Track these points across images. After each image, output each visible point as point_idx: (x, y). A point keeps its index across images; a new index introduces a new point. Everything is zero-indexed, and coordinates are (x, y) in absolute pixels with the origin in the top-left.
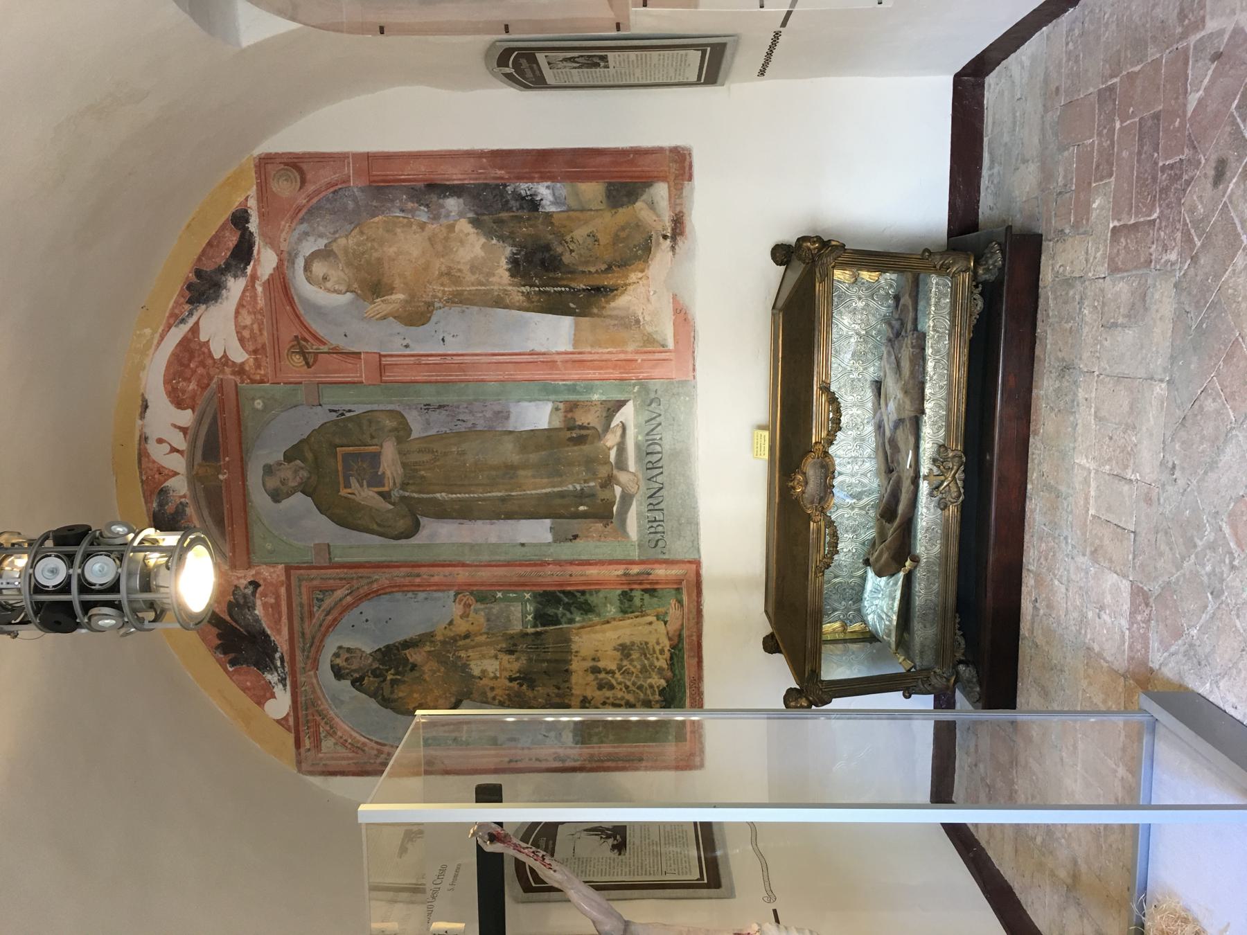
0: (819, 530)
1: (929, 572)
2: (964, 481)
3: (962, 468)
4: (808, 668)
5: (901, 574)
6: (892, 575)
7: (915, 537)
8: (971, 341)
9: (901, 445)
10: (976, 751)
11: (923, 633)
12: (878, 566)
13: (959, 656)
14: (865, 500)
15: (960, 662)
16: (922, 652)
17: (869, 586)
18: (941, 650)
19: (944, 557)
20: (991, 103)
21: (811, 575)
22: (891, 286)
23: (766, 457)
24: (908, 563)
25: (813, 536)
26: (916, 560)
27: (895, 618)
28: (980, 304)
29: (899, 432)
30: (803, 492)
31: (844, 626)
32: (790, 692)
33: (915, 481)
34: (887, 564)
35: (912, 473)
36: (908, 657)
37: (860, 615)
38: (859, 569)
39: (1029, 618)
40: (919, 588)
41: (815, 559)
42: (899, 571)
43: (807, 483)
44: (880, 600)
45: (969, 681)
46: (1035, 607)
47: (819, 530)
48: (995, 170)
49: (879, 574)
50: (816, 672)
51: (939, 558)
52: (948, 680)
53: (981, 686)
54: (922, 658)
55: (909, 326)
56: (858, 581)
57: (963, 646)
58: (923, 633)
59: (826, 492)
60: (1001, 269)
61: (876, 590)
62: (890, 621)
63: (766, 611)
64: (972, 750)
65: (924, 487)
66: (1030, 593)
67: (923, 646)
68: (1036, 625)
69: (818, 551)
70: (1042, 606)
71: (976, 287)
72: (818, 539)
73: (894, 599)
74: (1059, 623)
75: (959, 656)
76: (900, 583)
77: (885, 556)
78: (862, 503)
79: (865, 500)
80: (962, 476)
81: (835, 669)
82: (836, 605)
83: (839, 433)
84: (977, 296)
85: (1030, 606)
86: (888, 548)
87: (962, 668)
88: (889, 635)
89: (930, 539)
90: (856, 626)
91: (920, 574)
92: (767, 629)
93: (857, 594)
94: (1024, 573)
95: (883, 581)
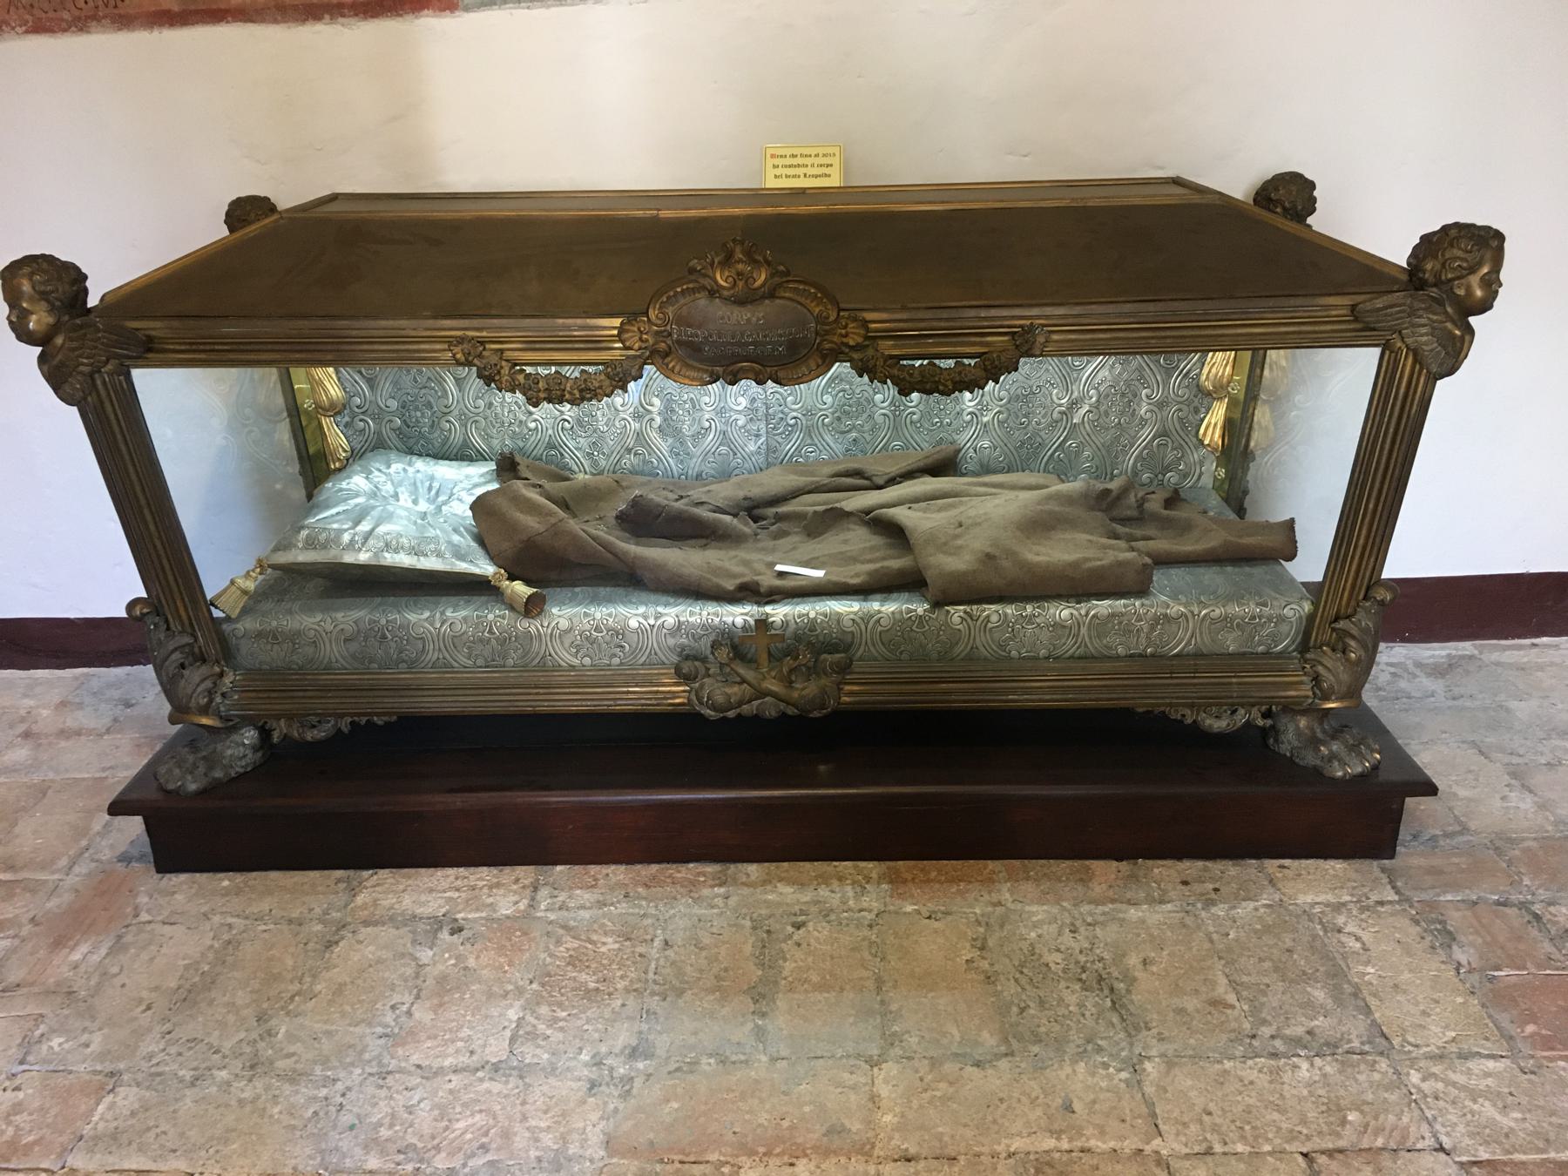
0: (595, 344)
1: (503, 642)
2: (756, 719)
3: (791, 711)
4: (155, 327)
5: (486, 568)
6: (480, 541)
7: (595, 600)
8: (1128, 712)
9: (832, 543)
10: (64, 734)
11: (330, 627)
12: (503, 504)
13: (280, 729)
14: (662, 445)
15: (265, 733)
16: (273, 636)
17: (446, 471)
18: (281, 683)
19: (544, 673)
20: (1552, 656)
21: (452, 327)
22: (1185, 476)
23: (771, 183)
24: (521, 589)
25: (574, 326)
26: (533, 607)
27: (363, 557)
28: (1219, 725)
29: (858, 538)
30: (714, 292)
31: (335, 410)
32: (74, 277)
33: (748, 592)
34: (511, 528)
35: (767, 581)
36: (253, 603)
37: (368, 448)
38: (487, 437)
39: (407, 902)
40: (457, 616)
41: (508, 335)
42: (493, 558)
43: (741, 302)
44: (411, 510)
45: (211, 761)
46: (437, 923)
47: (595, 344)
48: (1428, 683)
49: (479, 506)
50: (153, 352)
51: (542, 667)
52: (204, 710)
53: (201, 793)
54: (260, 635)
55: (1162, 545)
56: (456, 437)
57: (310, 736)
58: (330, 627)
59: (714, 361)
60: (1317, 774)
61: (437, 494)
62: (351, 545)
63: (334, 198)
64: (72, 720)
65: (738, 615)
66: (473, 902)
67: (295, 637)
68: (387, 933)
69: (531, 345)
70: (436, 958)
71: (1267, 715)
72: (567, 343)
73: (417, 553)
74: (395, 1039)
75: (280, 729)
76: (462, 567)
77: (531, 523)
78: (654, 435)
79: (662, 445)
80: (771, 713)
81: (186, 409)
82: (386, 387)
83: (890, 390)
84: (1241, 717)
85: (433, 906)
86: (556, 530)
87: (249, 736)
88: (311, 544)
89: (592, 641)
90: (337, 437)
91: (495, 616)
92: (286, 198)
93: (421, 440)
94: (526, 873)
95: (461, 509)
